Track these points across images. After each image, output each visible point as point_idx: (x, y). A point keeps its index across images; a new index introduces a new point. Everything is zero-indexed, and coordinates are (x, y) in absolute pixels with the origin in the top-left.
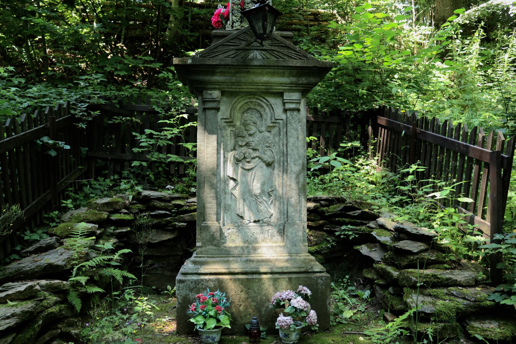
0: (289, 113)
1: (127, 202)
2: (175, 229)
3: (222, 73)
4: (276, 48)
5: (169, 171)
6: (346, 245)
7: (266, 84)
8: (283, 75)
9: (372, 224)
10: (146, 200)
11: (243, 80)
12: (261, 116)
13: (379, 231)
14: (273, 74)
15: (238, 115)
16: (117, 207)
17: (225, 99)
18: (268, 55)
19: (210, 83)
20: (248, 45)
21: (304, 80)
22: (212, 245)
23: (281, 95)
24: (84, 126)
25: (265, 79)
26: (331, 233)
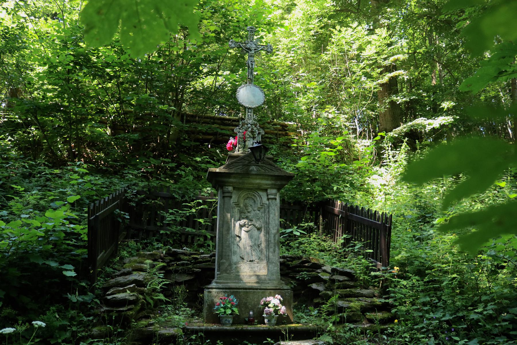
0: (270, 201)
1: (162, 255)
2: (193, 273)
3: (235, 178)
4: (264, 165)
5: (181, 239)
6: (303, 284)
7: (258, 184)
8: (268, 180)
9: (319, 271)
10: (175, 254)
11: (246, 181)
12: (255, 202)
13: (323, 273)
14: (262, 179)
15: (242, 201)
16: (156, 258)
17: (235, 191)
18: (260, 169)
19: (228, 182)
20: (249, 163)
21: (279, 183)
22: (226, 273)
23: (266, 190)
24: (134, 205)
25: (258, 181)
26: (293, 278)
